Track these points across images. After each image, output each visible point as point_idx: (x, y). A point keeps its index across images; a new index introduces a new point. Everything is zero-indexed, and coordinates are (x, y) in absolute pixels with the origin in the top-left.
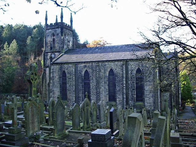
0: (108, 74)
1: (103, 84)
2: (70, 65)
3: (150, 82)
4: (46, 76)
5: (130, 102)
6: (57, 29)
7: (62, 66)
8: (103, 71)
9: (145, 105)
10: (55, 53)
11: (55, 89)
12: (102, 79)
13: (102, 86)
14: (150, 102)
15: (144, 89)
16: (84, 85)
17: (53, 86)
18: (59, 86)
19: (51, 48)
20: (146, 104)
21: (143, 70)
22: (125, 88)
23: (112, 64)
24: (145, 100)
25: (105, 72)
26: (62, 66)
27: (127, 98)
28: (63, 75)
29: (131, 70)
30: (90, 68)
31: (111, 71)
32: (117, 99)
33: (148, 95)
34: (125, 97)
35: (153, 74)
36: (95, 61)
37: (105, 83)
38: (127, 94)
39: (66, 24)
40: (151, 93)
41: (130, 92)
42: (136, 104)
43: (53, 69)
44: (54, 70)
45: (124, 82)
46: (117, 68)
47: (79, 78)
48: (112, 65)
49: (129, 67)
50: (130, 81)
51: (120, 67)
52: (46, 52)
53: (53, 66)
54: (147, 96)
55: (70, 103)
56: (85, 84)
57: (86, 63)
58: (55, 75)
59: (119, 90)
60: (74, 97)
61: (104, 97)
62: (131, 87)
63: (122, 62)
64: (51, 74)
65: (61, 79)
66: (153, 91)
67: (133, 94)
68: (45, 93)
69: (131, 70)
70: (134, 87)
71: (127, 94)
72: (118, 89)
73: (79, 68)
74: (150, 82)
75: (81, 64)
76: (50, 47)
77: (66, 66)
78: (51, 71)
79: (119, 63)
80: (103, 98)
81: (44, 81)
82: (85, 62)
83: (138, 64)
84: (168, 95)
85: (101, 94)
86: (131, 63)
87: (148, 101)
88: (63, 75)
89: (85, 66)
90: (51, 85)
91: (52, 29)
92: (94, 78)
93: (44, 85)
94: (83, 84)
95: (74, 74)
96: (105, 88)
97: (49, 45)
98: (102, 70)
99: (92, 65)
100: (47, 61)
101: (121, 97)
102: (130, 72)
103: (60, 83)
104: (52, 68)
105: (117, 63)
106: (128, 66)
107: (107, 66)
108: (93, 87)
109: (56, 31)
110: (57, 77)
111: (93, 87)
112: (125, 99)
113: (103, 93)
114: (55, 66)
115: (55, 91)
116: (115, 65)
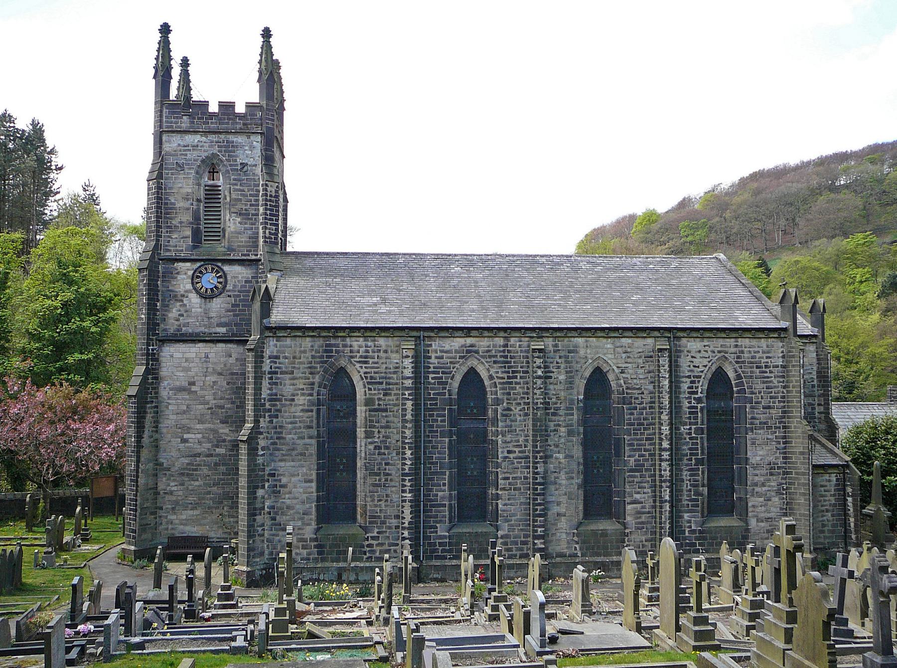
0: (582, 390)
1: (563, 440)
2: (382, 342)
3: (770, 428)
4: (156, 389)
5: (686, 516)
6: (240, 139)
7: (333, 342)
8: (562, 377)
9: (747, 530)
10: (226, 268)
11: (284, 467)
12: (554, 414)
13: (557, 446)
14: (769, 515)
15: (747, 459)
16: (459, 442)
17: (274, 447)
18: (313, 450)
19: (197, 238)
20: (753, 523)
21: (739, 377)
22: (666, 455)
23: (608, 344)
24: (750, 504)
25: (570, 383)
26: (333, 342)
27: (675, 502)
28: (337, 392)
29: (689, 377)
30: (495, 362)
31: (598, 378)
32: (629, 507)
33: (763, 485)
34: (667, 498)
35: (783, 397)
36: (610, 329)
37: (570, 433)
38: (675, 483)
39: (227, 107)
40: (771, 474)
41: (685, 475)
42: (712, 525)
43: (274, 358)
44: (284, 364)
45: (666, 429)
46: (625, 365)
47: (437, 409)
48: (607, 353)
49: (684, 362)
50: (685, 424)
51: (640, 361)
52: (164, 254)
53: (272, 342)
54: (757, 489)
55: (373, 538)
56: (462, 436)
57: (474, 333)
58: (287, 389)
59: (638, 468)
60: (408, 504)
61: (563, 499)
62: (690, 449)
63: (650, 341)
64: (265, 383)
65: (323, 408)
66: (779, 468)
67: (694, 481)
68: (151, 485)
69: (689, 377)
70: (702, 453)
71: (675, 483)
72: (632, 459)
73: (433, 360)
74: (770, 428)
75: (448, 341)
76: (188, 232)
77: (357, 343)
78: (266, 367)
79: (639, 342)
80: (559, 504)
81: (149, 417)
82: (467, 331)
83: (719, 352)
84: (830, 481)
85: (552, 488)
86: (692, 345)
87: (761, 512)
88: (337, 392)
89: (470, 351)
90: (262, 443)
91: (206, 133)
92: (516, 410)
93: (146, 440)
94: (455, 437)
95: (408, 389)
96: (569, 457)
97: (187, 217)
98: (559, 373)
99: (506, 346)
100: (166, 306)
101: (644, 496)
102: (685, 387)
103: (319, 436)
104: (267, 353)
105: (629, 341)
106: (679, 357)
107: (582, 352)
108: (509, 452)
109: (230, 148)
110: (301, 400)
111: (509, 452)
112: (667, 507)
113: (563, 479)
114: (288, 341)
115: (284, 480)
116: (619, 350)
